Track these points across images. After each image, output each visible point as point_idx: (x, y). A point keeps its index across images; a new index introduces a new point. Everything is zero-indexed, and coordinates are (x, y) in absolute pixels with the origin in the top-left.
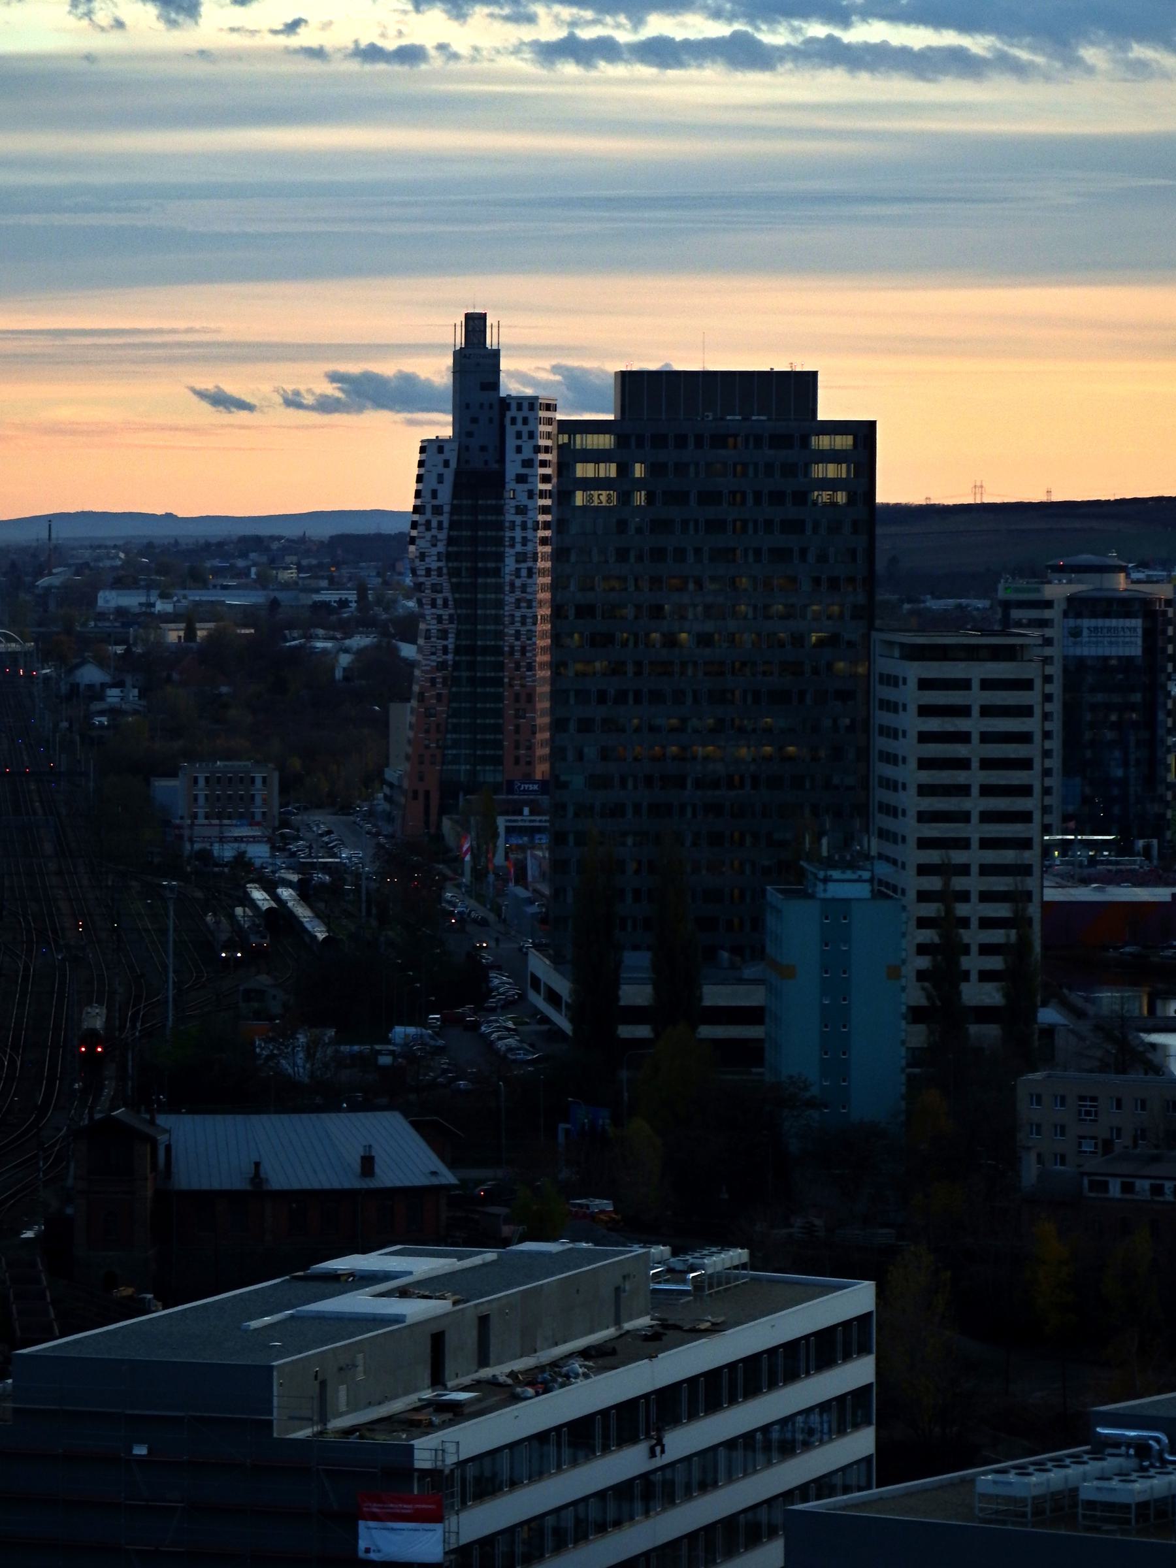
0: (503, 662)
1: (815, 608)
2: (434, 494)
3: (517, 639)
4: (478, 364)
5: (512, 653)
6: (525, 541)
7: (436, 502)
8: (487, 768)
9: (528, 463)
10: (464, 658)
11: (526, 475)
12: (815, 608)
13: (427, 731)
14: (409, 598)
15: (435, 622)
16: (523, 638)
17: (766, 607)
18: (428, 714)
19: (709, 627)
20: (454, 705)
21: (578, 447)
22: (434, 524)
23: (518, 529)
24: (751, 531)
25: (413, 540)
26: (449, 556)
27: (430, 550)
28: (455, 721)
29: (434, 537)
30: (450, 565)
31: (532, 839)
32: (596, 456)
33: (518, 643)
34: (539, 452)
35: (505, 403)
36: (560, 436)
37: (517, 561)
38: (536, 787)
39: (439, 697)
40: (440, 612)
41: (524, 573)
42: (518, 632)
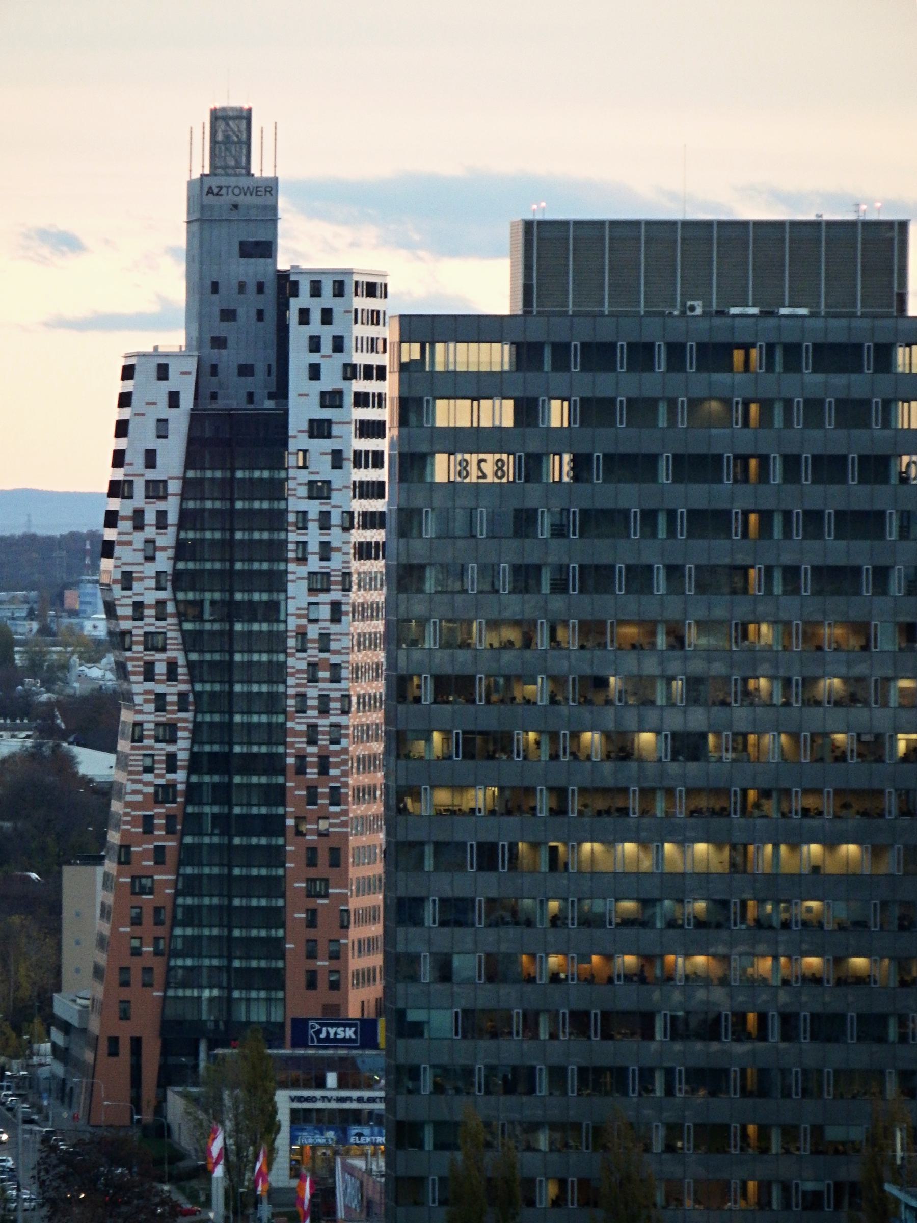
0: (283, 787)
1: (904, 683)
2: (150, 458)
3: (312, 741)
4: (236, 207)
5: (301, 770)
6: (326, 551)
7: (151, 475)
8: (254, 994)
9: (332, 399)
10: (207, 779)
11: (329, 422)
12: (904, 683)
13: (136, 921)
14: (94, 660)
15: (151, 707)
16: (323, 740)
17: (809, 682)
18: (139, 886)
19: (697, 719)
20: (189, 870)
21: (439, 368)
22: (150, 517)
23: (313, 527)
24: (777, 533)
25: (108, 549)
26: (179, 580)
27: (145, 562)
28: (189, 901)
29: (150, 542)
30: (181, 596)
31: (343, 1139)
32: (477, 386)
33: (313, 749)
34: (354, 377)
35: (286, 284)
36: (405, 346)
37: (312, 590)
38: (350, 1033)
39: (159, 854)
40: (160, 688)
41: (325, 612)
42: (313, 727)
